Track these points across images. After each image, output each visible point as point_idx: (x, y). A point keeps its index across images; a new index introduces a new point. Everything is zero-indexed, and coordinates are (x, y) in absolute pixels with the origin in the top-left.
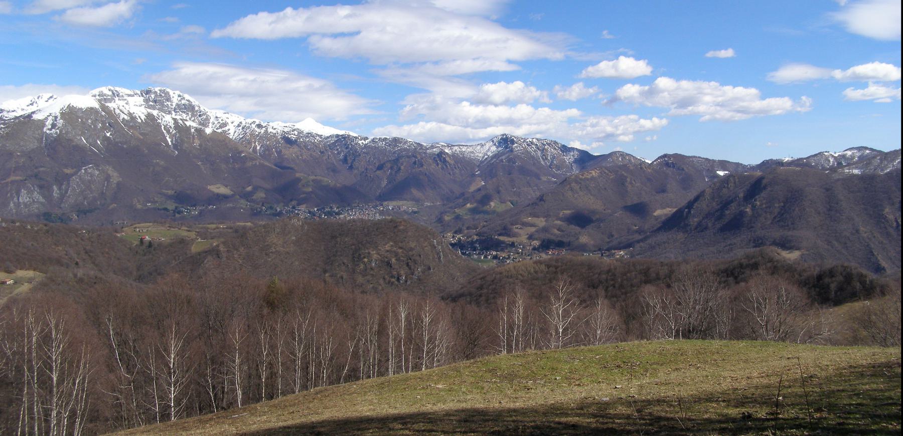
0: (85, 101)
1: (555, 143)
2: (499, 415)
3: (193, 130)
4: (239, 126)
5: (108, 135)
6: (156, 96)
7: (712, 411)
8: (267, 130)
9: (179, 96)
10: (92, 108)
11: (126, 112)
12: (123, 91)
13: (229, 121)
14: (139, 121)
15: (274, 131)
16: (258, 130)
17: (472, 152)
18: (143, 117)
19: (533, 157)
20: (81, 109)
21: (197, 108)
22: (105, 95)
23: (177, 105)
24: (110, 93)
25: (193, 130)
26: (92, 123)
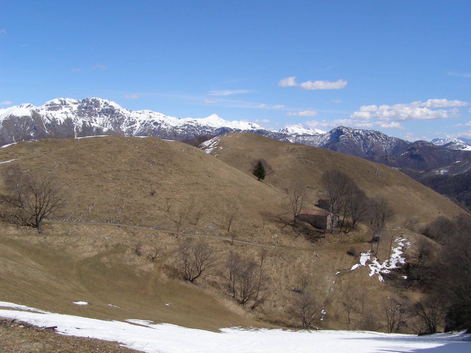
0: (22, 111)
1: (378, 133)
2: (54, 311)
3: (94, 129)
4: (143, 124)
5: (32, 134)
6: (87, 104)
7: (141, 322)
8: (160, 127)
9: (106, 103)
10: (26, 117)
11: (51, 118)
12: (68, 100)
13: (137, 120)
14: (59, 124)
15: (165, 127)
16: (154, 127)
17: (313, 142)
18: (63, 121)
19: (355, 146)
20: (19, 117)
21: (116, 111)
22: (55, 104)
23: (102, 110)
24: (60, 103)
25: (94, 129)
26: (23, 127)
